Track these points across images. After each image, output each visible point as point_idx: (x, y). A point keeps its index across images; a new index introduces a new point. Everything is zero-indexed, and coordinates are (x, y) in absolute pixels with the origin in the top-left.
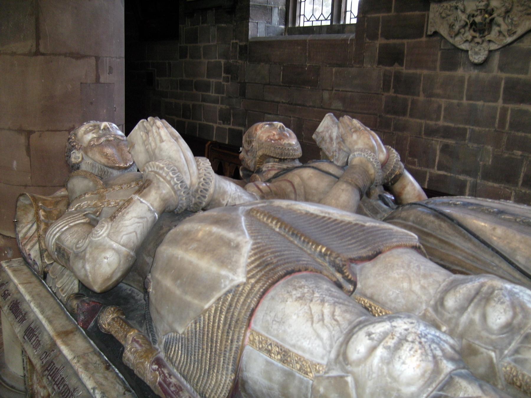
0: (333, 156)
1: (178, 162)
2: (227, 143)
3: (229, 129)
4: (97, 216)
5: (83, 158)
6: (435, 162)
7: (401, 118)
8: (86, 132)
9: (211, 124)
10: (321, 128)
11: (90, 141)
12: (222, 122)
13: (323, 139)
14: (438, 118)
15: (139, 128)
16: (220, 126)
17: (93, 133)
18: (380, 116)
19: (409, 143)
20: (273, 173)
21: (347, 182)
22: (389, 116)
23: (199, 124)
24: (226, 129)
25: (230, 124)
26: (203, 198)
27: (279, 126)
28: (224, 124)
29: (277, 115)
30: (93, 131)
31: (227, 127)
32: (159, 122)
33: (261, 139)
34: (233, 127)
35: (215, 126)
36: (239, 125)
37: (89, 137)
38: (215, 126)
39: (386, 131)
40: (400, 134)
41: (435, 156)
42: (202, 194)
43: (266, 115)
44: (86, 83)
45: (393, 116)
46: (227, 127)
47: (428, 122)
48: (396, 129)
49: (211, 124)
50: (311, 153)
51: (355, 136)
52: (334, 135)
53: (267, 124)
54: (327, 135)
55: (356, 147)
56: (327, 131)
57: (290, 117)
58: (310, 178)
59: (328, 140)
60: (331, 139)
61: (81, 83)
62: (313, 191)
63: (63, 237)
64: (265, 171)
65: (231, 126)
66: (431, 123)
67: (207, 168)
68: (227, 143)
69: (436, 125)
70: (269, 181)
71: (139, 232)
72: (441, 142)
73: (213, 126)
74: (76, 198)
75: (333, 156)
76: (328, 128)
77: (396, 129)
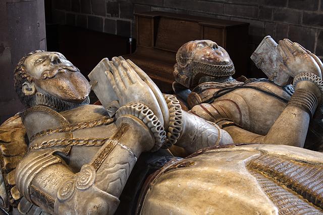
0: (274, 77)
1: (152, 104)
2: (116, 34)
3: (118, 21)
4: (67, 156)
5: (36, 91)
6: (314, 48)
7: (280, 8)
8: (37, 63)
9: (100, 16)
10: (260, 49)
11: (43, 74)
12: (110, 15)
13: (263, 60)
14: (316, 8)
15: (102, 66)
16: (108, 18)
17: (44, 65)
18: (260, 7)
19: (288, 30)
20: (213, 92)
21: (297, 106)
22: (269, 7)
23: (88, 16)
24: (114, 21)
25: (118, 16)
26: (175, 137)
27: (212, 45)
28: (112, 16)
29: (163, 7)
30: (44, 63)
31: (116, 19)
32: (126, 63)
33: (196, 58)
34: (121, 19)
35: (104, 18)
36: (127, 17)
37: (40, 69)
38: (104, 18)
39: (267, 20)
40: (280, 23)
41: (314, 42)
42: (174, 133)
43: (152, 7)
44: (12, 3)
45: (273, 7)
46: (116, 19)
47: (306, 11)
48: (276, 19)
49: (100, 16)
50: (248, 70)
51: (298, 60)
52: (274, 57)
53: (199, 43)
54: (267, 57)
55: (300, 71)
56: (267, 53)
57: (176, 9)
58: (253, 98)
59: (268, 61)
60: (271, 61)
61: (7, 3)
62: (259, 111)
63: (39, 180)
64: (205, 90)
65: (119, 19)
66: (310, 12)
67: (178, 107)
68: (116, 34)
69: (314, 14)
70: (210, 101)
71: (123, 177)
72: (319, 29)
73: (102, 18)
74: (38, 133)
75: (274, 77)
76: (268, 49)
77: (276, 19)
